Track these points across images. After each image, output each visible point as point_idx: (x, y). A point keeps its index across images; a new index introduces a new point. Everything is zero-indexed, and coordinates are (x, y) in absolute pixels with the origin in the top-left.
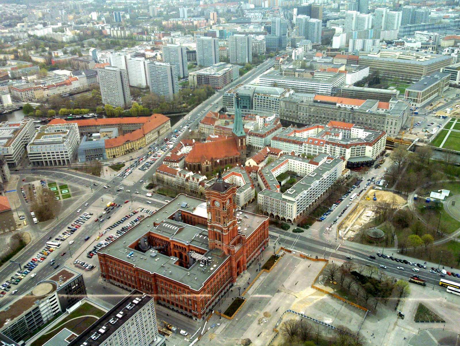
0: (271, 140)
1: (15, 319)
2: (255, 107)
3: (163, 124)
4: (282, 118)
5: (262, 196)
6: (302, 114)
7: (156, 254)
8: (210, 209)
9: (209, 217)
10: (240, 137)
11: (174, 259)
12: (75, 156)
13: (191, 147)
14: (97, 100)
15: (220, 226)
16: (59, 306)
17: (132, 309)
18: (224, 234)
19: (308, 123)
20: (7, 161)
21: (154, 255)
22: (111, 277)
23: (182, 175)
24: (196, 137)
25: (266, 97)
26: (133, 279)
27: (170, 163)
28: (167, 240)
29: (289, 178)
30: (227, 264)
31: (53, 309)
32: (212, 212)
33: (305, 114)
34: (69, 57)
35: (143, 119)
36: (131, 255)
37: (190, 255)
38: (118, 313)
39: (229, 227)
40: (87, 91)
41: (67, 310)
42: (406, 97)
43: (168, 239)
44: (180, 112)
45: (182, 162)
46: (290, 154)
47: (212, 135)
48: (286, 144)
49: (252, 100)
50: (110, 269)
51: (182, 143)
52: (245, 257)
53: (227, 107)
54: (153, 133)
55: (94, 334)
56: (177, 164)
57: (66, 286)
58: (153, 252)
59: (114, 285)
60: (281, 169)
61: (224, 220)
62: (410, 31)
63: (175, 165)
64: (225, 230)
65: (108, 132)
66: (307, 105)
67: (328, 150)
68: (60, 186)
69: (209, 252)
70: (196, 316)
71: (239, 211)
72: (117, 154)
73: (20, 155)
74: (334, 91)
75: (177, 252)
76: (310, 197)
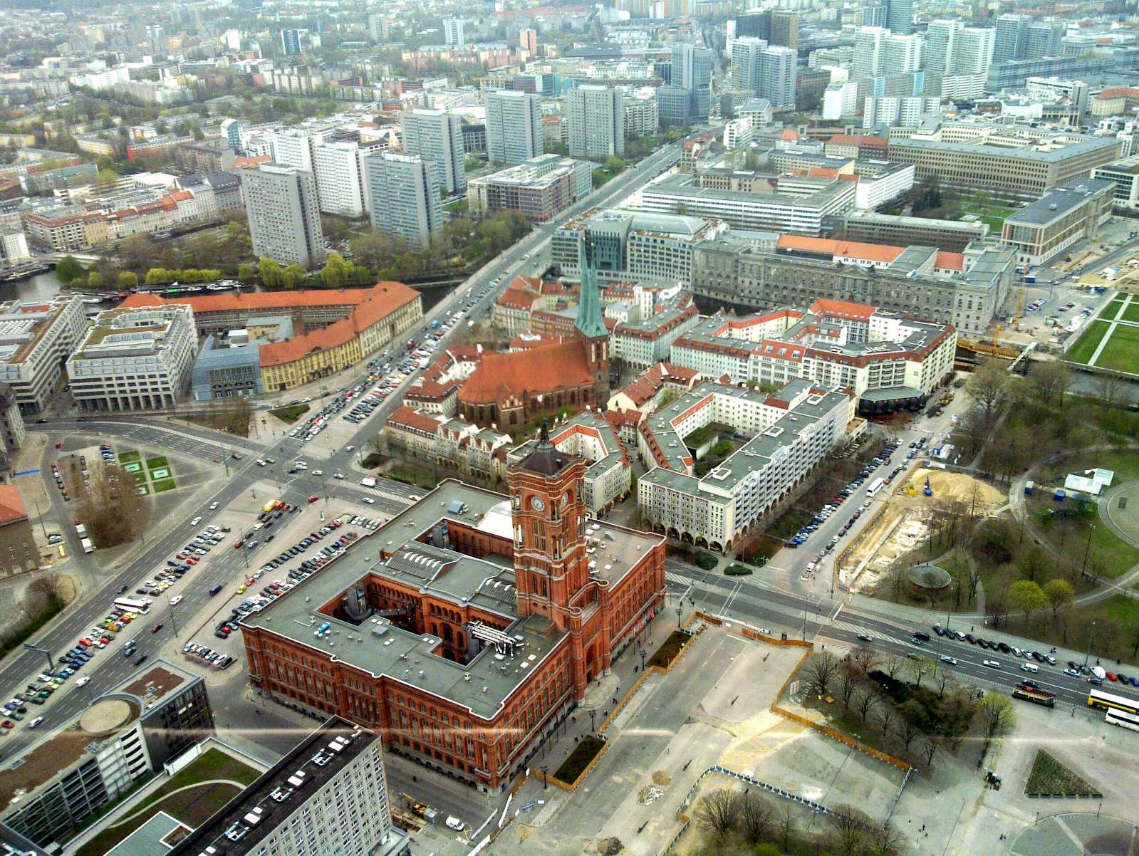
0: (672, 347)
1: (38, 789)
2: (632, 265)
3: (403, 306)
4: (698, 292)
5: (649, 484)
6: (747, 281)
7: (386, 629)
8: (519, 518)
9: (518, 537)
10: (593, 340)
11: (431, 642)
12: (186, 387)
13: (473, 363)
14: (241, 248)
15: (544, 558)
16: (146, 758)
17: (327, 763)
18: (555, 579)
19: (762, 304)
20: (18, 398)
21: (380, 630)
22: (274, 686)
23: (451, 434)
24: (486, 340)
25: (659, 240)
26: (329, 689)
27: (420, 404)
28: (413, 593)
29: (716, 440)
30: (562, 654)
31: (130, 764)
32: (525, 525)
33: (755, 282)
34: (170, 142)
35: (353, 295)
36: (323, 631)
37: (471, 631)
38: (293, 773)
39: (566, 562)
40: (216, 224)
41: (166, 767)
42: (1006, 240)
43: (417, 590)
44: (447, 278)
45: (450, 401)
46: (718, 381)
47: (526, 333)
48: (708, 357)
49: (625, 247)
50: (272, 666)
51: (450, 354)
52: (607, 637)
53: (561, 264)
54: (378, 330)
55: (234, 827)
56: (439, 405)
57: (163, 709)
58: (380, 623)
59: (282, 704)
60: (695, 418)
61: (554, 544)
62: (1016, 77)
63: (433, 407)
64: (556, 569)
65: (266, 326)
66: (760, 261)
67: (811, 371)
68: (147, 461)
69: (517, 624)
70: (485, 781)
71: (591, 522)
72: (290, 380)
73: (50, 384)
74: (828, 225)
75: (438, 622)
76: (768, 488)
